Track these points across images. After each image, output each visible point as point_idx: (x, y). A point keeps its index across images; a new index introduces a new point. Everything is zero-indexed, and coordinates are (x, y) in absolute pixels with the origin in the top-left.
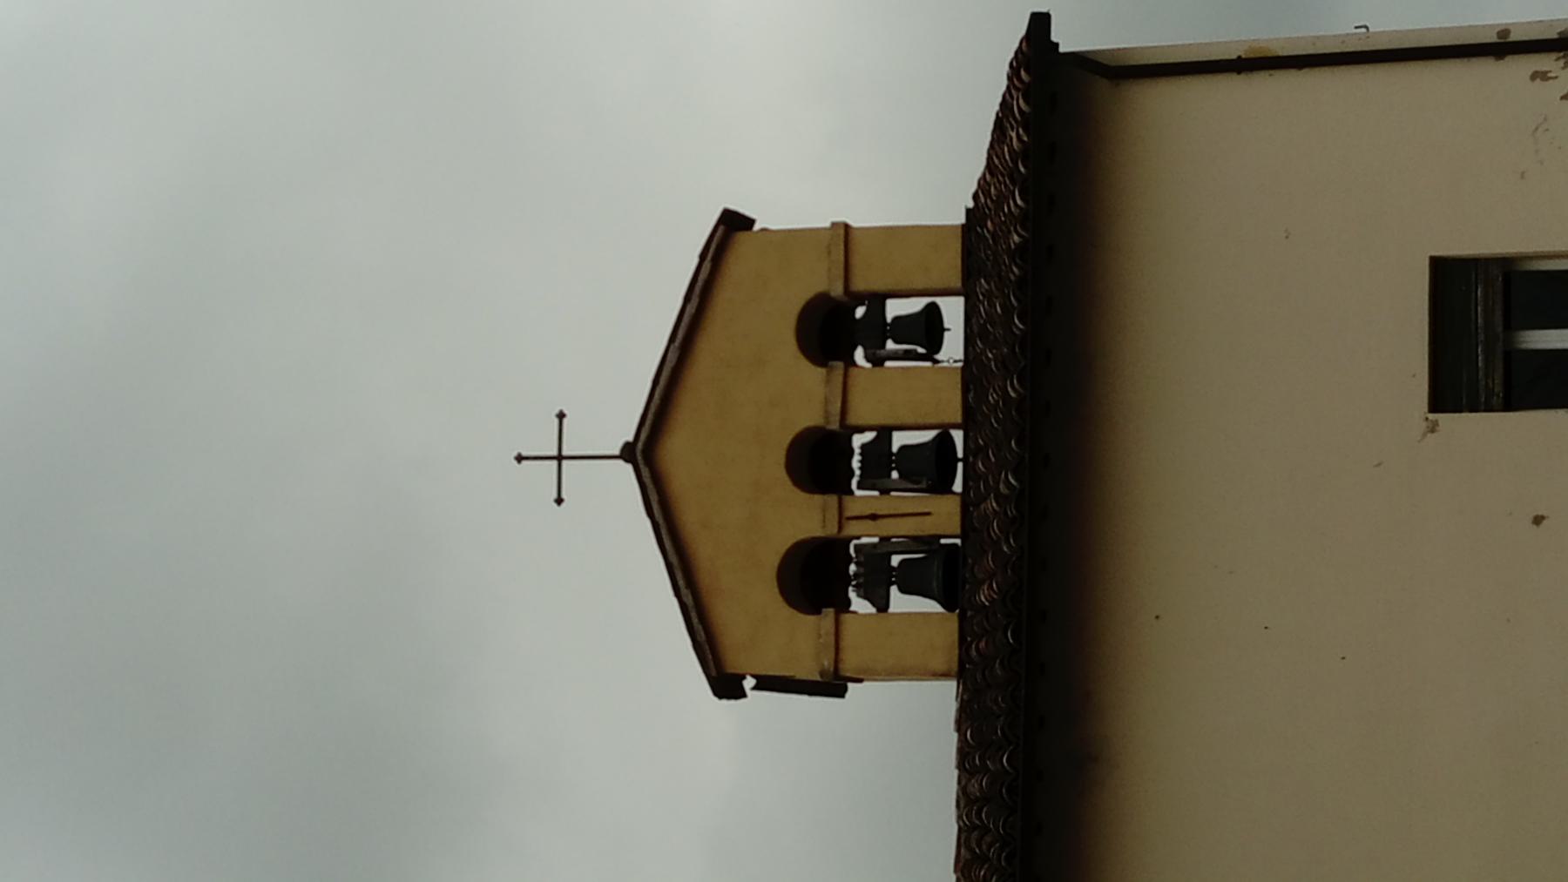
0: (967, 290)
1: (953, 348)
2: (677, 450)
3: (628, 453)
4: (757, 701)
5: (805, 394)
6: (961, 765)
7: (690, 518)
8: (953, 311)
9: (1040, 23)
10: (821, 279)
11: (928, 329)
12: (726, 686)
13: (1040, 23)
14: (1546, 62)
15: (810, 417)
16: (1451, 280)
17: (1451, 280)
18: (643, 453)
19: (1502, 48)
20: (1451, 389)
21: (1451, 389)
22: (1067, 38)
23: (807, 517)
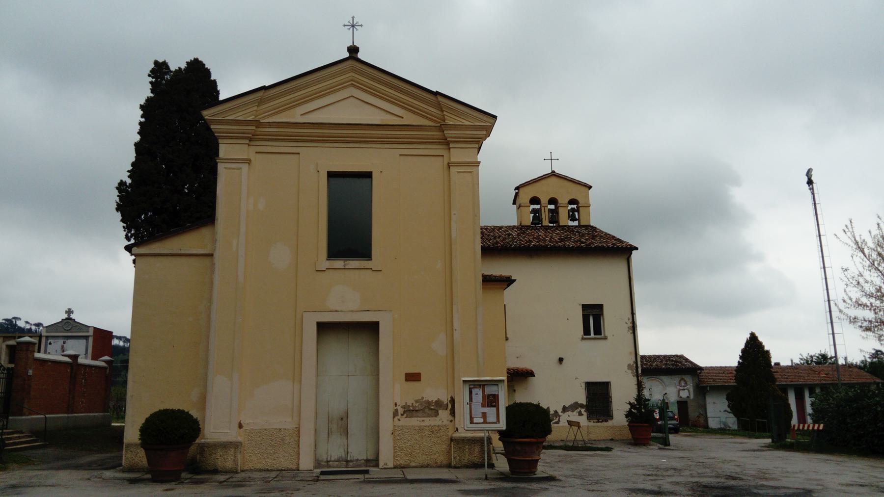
0: (580, 226)
1: (571, 223)
2: (554, 179)
3: (553, 172)
4: (514, 192)
5: (563, 200)
6: (665, 357)
7: (543, 182)
8: (576, 223)
9: (636, 249)
10: (582, 202)
11: (573, 219)
12: (517, 188)
13: (636, 249)
14: (631, 320)
15: (560, 201)
16: (600, 307)
17: (600, 307)
18: (553, 174)
19: (633, 314)
20: (585, 307)
21: (585, 307)
22: (634, 252)
23: (544, 200)
